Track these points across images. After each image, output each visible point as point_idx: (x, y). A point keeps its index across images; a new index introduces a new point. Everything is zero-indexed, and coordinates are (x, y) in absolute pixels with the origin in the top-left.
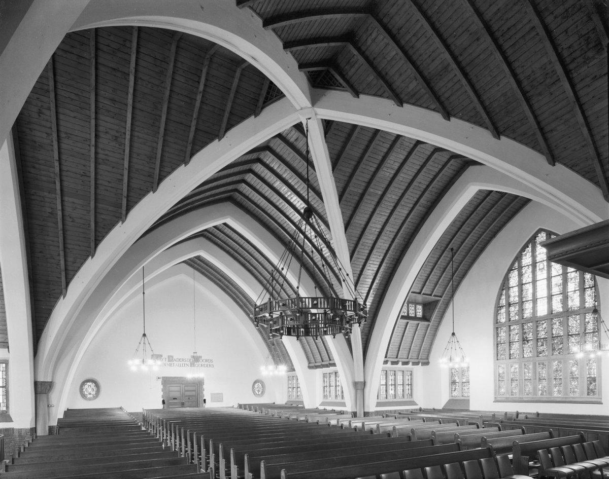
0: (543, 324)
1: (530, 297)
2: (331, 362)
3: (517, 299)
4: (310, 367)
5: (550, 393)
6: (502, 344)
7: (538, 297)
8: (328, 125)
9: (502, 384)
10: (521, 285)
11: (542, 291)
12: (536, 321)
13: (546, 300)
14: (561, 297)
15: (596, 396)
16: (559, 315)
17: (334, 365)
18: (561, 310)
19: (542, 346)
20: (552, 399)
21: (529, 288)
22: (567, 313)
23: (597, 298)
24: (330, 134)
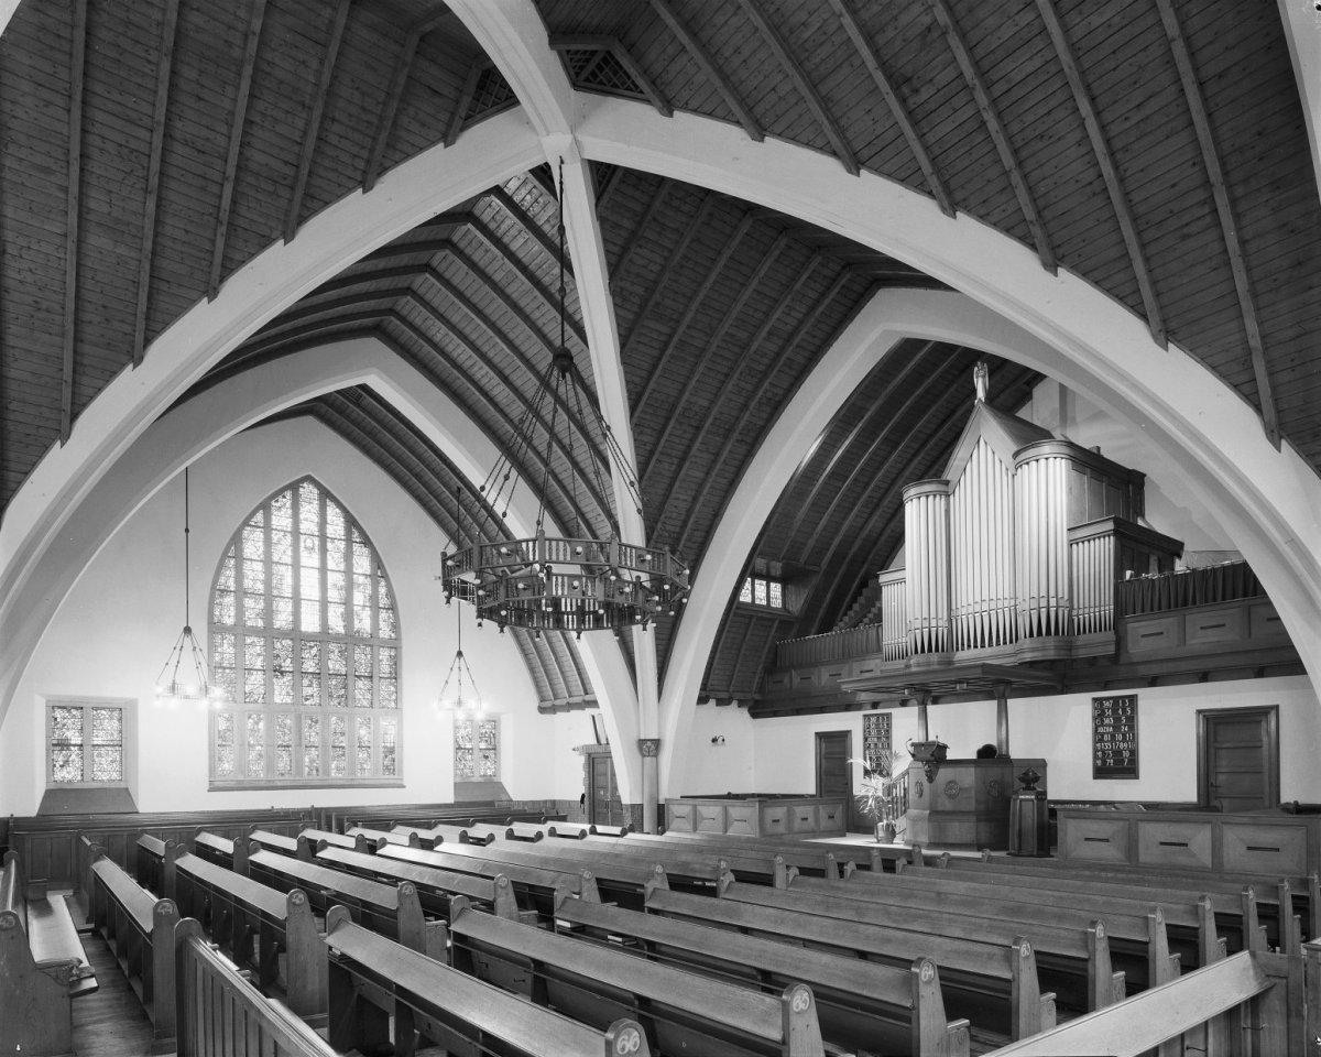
0: (311, 647)
1: (288, 592)
2: (588, 698)
3: (260, 587)
4: (542, 710)
5: (326, 771)
6: (224, 668)
7: (303, 597)
8: (604, 176)
9: (226, 752)
10: (268, 562)
11: (310, 589)
12: (295, 635)
13: (317, 606)
14: (341, 609)
15: (396, 777)
16: (337, 638)
17: (594, 704)
18: (342, 630)
19: (310, 686)
20: (330, 782)
21: (335, 579)
22: (350, 640)
23: (395, 627)
24: (606, 197)
